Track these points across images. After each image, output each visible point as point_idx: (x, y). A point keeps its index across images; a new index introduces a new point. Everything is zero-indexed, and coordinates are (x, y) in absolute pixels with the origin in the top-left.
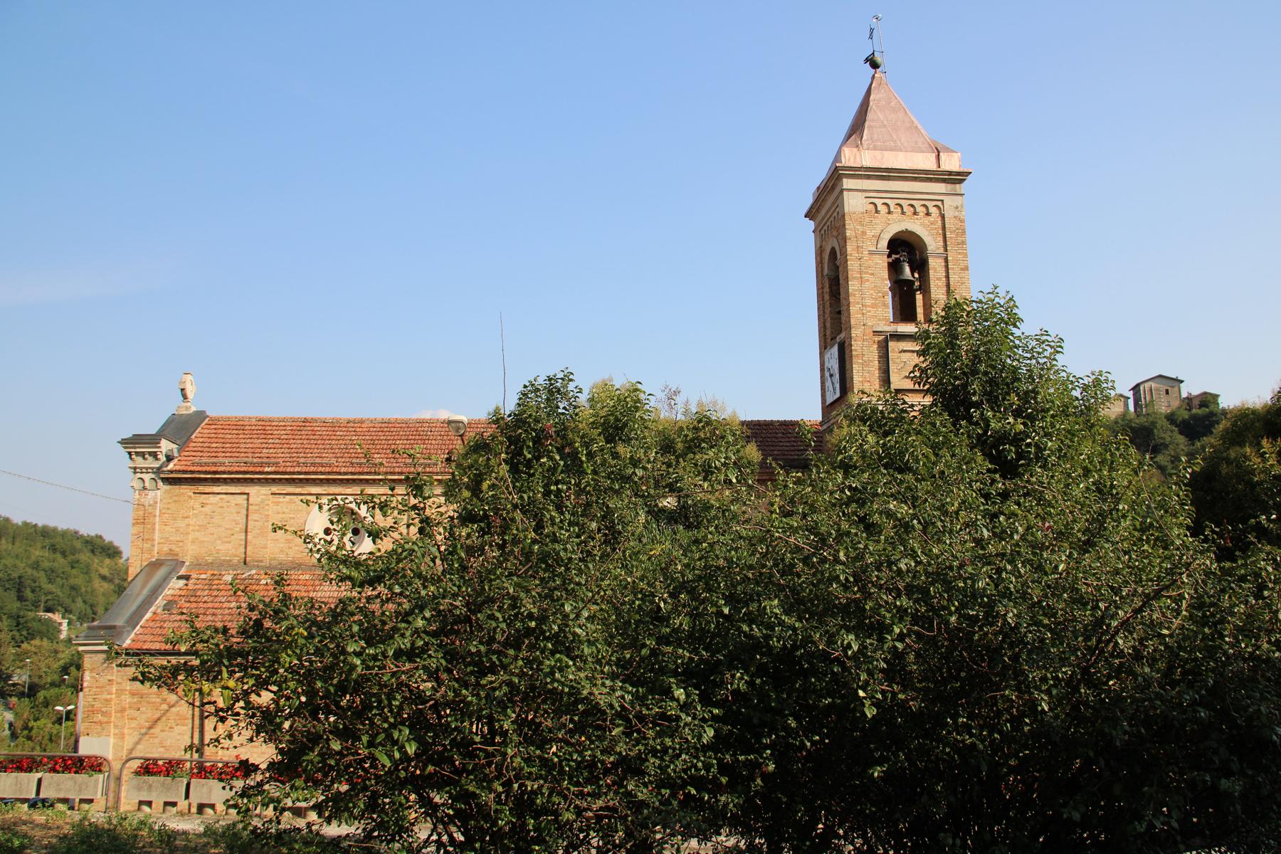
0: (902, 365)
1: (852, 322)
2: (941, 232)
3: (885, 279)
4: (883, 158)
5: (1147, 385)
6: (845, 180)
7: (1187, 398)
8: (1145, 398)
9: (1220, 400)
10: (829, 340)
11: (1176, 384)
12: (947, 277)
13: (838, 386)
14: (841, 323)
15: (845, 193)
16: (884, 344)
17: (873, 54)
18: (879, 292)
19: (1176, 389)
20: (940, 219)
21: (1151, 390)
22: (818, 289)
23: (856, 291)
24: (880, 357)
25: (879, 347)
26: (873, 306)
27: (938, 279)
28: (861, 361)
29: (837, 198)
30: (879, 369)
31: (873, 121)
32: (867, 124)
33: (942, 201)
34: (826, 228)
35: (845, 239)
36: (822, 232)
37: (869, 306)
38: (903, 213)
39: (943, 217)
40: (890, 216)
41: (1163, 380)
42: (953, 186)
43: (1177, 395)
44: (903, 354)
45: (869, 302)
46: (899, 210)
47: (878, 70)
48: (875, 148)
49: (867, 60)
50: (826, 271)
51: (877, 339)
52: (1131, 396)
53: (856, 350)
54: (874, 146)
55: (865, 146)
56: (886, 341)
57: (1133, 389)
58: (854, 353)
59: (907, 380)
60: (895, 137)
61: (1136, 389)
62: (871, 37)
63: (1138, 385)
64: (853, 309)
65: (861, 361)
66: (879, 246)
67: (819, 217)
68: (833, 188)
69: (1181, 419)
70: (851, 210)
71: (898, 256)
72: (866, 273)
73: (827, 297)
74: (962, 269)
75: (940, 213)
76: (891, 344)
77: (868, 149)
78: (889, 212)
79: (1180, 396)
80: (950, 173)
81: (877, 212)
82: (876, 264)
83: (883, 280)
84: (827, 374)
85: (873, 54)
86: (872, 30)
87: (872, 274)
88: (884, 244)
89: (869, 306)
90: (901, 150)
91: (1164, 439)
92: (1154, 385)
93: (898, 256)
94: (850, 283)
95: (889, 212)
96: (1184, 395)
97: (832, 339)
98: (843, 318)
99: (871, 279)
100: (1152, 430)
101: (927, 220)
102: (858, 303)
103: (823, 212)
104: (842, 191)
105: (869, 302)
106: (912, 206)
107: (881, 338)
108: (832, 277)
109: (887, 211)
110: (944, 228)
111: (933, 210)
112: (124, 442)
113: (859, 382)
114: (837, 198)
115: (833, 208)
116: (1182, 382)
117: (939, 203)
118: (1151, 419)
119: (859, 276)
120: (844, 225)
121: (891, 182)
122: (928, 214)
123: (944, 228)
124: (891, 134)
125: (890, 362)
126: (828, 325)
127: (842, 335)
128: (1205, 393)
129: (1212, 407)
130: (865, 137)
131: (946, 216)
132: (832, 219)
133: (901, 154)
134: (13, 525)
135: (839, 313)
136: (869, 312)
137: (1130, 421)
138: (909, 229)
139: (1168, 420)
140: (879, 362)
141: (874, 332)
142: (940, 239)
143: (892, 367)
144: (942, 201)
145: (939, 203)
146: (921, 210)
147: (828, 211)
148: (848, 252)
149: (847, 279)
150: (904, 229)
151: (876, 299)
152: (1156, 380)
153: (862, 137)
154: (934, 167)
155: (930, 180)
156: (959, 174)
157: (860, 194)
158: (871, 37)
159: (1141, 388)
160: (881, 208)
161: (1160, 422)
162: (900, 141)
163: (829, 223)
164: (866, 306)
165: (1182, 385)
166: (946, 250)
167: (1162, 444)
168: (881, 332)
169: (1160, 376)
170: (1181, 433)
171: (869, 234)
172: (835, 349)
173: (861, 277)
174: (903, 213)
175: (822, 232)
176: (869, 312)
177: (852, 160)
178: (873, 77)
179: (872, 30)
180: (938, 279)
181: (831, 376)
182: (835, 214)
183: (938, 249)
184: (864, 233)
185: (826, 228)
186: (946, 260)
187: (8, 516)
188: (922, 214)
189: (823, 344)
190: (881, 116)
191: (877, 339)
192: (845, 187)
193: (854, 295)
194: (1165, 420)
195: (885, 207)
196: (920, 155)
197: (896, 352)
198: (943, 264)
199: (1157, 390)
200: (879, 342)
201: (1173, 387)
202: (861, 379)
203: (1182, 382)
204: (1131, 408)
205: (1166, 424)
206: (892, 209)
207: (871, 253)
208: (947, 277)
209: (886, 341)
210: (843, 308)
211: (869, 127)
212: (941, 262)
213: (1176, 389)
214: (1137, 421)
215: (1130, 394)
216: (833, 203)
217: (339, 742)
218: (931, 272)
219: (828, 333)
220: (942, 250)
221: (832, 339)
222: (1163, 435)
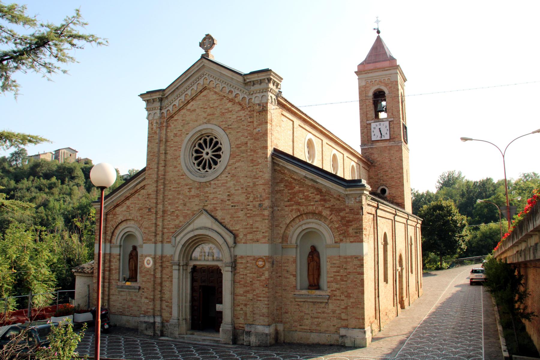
5: (63, 151)
7: (78, 159)
9: (431, 191)
11: (75, 152)
21: (64, 153)
41: (70, 150)
57: (55, 151)
63: (59, 150)
92: (66, 151)
96: (77, 158)
112: (142, 95)
116: (77, 152)
128: (87, 159)
129: (90, 164)
134: (433, 195)
159: (60, 152)
165: (77, 153)
169: (69, 148)
187: (85, 157)
199: (67, 153)
203: (77, 152)
217: (241, 337)
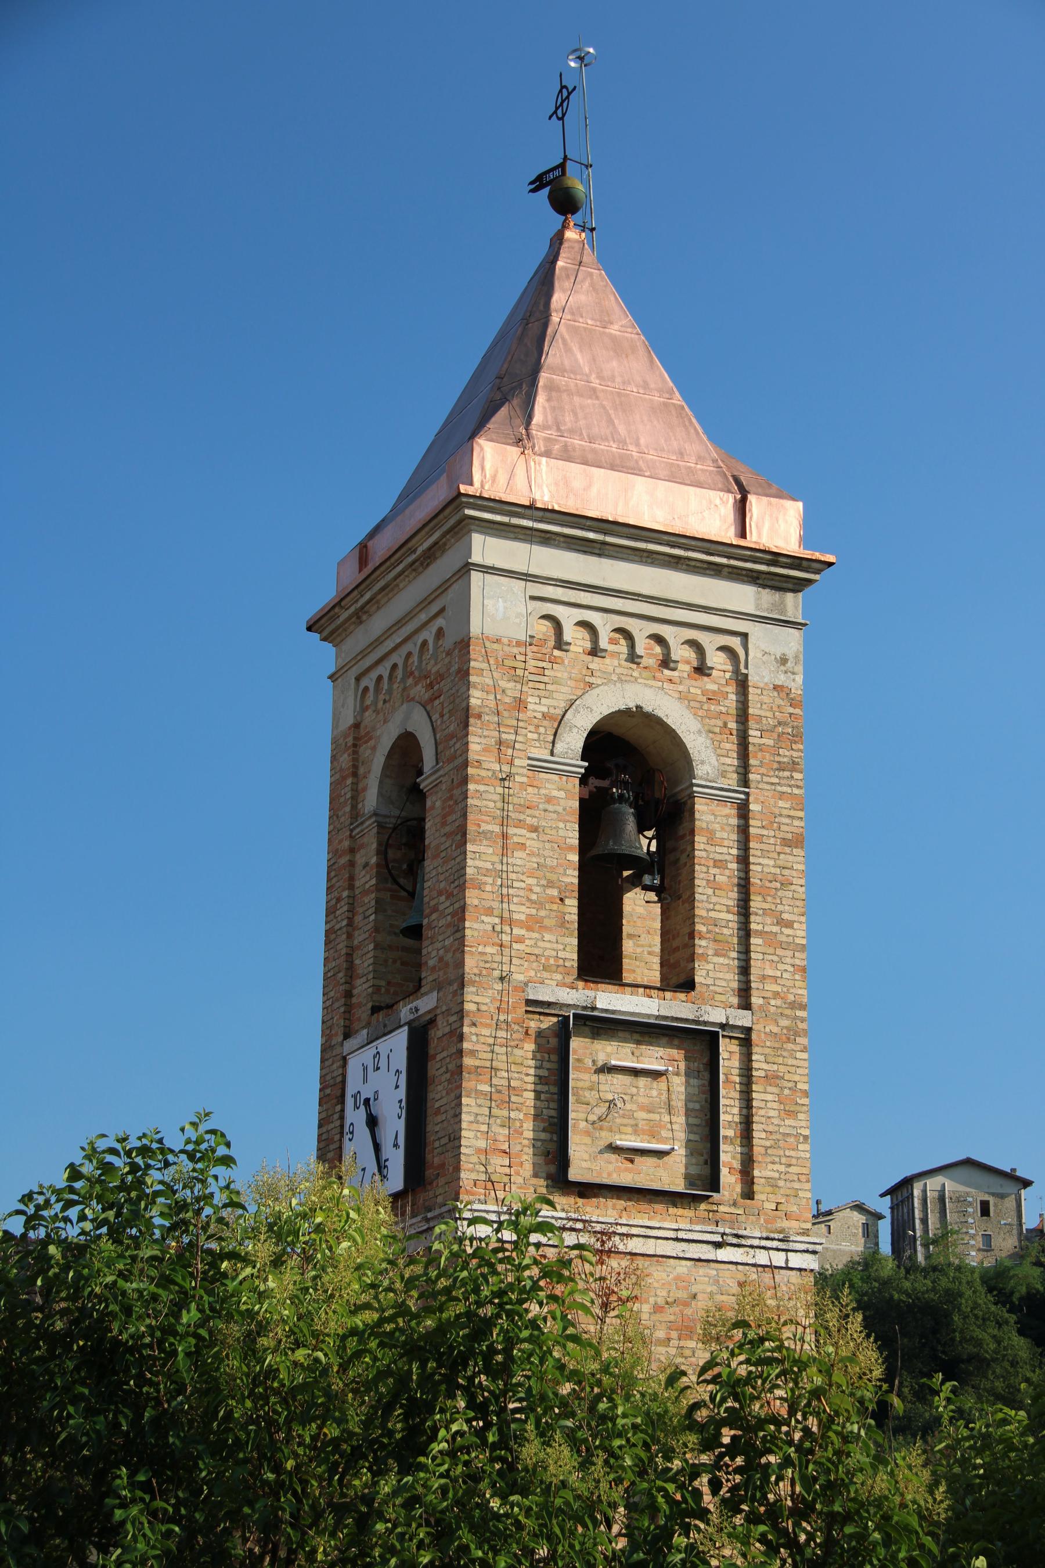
0: (601, 1110)
1: (470, 964)
2: (733, 725)
3: (570, 848)
4: (588, 488)
5: (933, 1184)
6: (477, 539)
8: (924, 1221)
10: (363, 1013)
11: (1010, 1187)
12: (744, 860)
13: (396, 1159)
14: (419, 966)
15: (475, 577)
16: (554, 1042)
17: (562, 166)
18: (550, 884)
19: (1010, 1203)
20: (731, 689)
21: (942, 1199)
22: (334, 853)
23: (487, 873)
24: (540, 1080)
25: (539, 1049)
26: (533, 924)
27: (717, 864)
28: (486, 1088)
29: (444, 587)
30: (537, 1117)
31: (561, 371)
32: (544, 377)
33: (745, 636)
34: (384, 670)
35: (464, 716)
36: (369, 681)
37: (521, 924)
38: (633, 657)
39: (742, 684)
40: (595, 663)
42: (777, 595)
43: (1012, 1219)
44: (602, 1077)
45: (521, 912)
46: (623, 647)
47: (572, 220)
48: (567, 455)
49: (539, 183)
50: (371, 800)
51: (534, 1024)
52: (887, 1213)
53: (473, 1053)
54: (565, 448)
55: (540, 446)
56: (563, 1033)
57: (891, 1192)
58: (468, 1061)
59: (613, 1157)
60: (622, 429)
61: (901, 1191)
62: (559, 112)
63: (907, 1183)
64: (475, 928)
65: (486, 1088)
66: (559, 747)
67: (359, 639)
68: (430, 556)
69: (1024, 1290)
70: (490, 631)
71: (605, 783)
72: (520, 824)
73: (366, 880)
74: (785, 842)
75: (736, 671)
76: (576, 1044)
77: (547, 454)
78: (595, 651)
79: (1020, 1225)
80: (775, 558)
81: (560, 644)
82: (549, 800)
83: (564, 848)
84: (356, 1117)
85: (562, 166)
86: (565, 94)
87: (534, 829)
88: (573, 742)
89: (521, 924)
90: (637, 471)
91: (979, 1343)
92: (950, 1185)
93: (605, 783)
94: (470, 847)
95: (595, 651)
97: (375, 1010)
98: (432, 952)
99: (532, 842)
100: (948, 1315)
101: (697, 687)
102: (489, 911)
103: (378, 623)
104: (467, 568)
105: (521, 912)
106: (659, 640)
107: (548, 1022)
108: (391, 823)
109: (588, 645)
110: (743, 716)
111: (716, 660)
113: (479, 1151)
114: (444, 587)
115: (423, 617)
116: (1026, 1183)
117: (735, 642)
118: (944, 1283)
119: (497, 829)
120: (464, 673)
121: (606, 563)
122: (701, 670)
123: (743, 716)
124: (610, 421)
125: (571, 1099)
126: (364, 963)
127: (426, 1003)
130: (538, 418)
131: (752, 679)
132: (413, 647)
133: (640, 484)
135: (415, 932)
136: (520, 940)
137: (886, 1283)
138: (648, 708)
139: (990, 1290)
140: (538, 1094)
141: (529, 1002)
142: (731, 746)
143: (575, 1114)
144: (745, 636)
145: (735, 642)
146: (681, 653)
147: (400, 623)
148: (472, 756)
149: (460, 836)
150: (632, 705)
151: (539, 905)
152: (949, 1172)
153: (529, 418)
154: (728, 534)
155: (715, 571)
156: (797, 562)
157: (518, 585)
158: (559, 112)
159: (917, 1192)
160: (570, 633)
161: (969, 1293)
162: (638, 445)
163: (397, 658)
164: (511, 923)
166: (745, 782)
167: (970, 1359)
168: (549, 1004)
170: (1021, 1332)
171: (536, 706)
172: (397, 1044)
173: (505, 836)
174: (633, 657)
175: (369, 681)
176: (520, 940)
177: (502, 479)
178: (558, 240)
179: (565, 94)
180: (717, 864)
181: (372, 1122)
182: (428, 635)
183: (723, 774)
184: (520, 704)
185: (384, 670)
186: (743, 811)
188: (685, 669)
189: (339, 1021)
190: (581, 358)
191: (534, 1024)
192: (476, 558)
193: (480, 887)
194: (982, 1290)
195: (583, 634)
196: (693, 492)
197: (586, 1070)
198: (734, 821)
199: (960, 1200)
200: (540, 1034)
201: (1002, 1196)
202: (482, 1144)
203: (1026, 1183)
204: (885, 1247)
205: (985, 1300)
206: (603, 643)
207: (536, 767)
208: (744, 860)
209: (563, 1033)
210: (435, 923)
211: (551, 388)
212: (729, 815)
213: (1010, 1203)
214: (907, 1285)
215: (884, 1206)
216: (426, 602)
218: (700, 841)
219: (362, 988)
220: (732, 780)
221: (375, 1010)
222: (978, 1333)
